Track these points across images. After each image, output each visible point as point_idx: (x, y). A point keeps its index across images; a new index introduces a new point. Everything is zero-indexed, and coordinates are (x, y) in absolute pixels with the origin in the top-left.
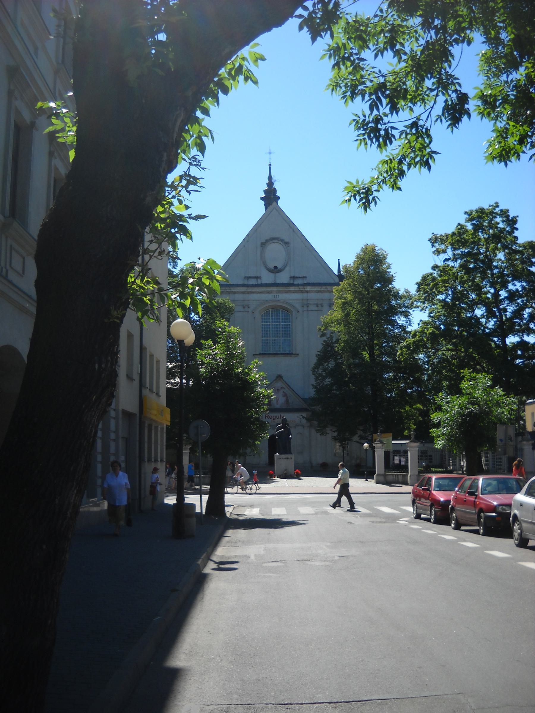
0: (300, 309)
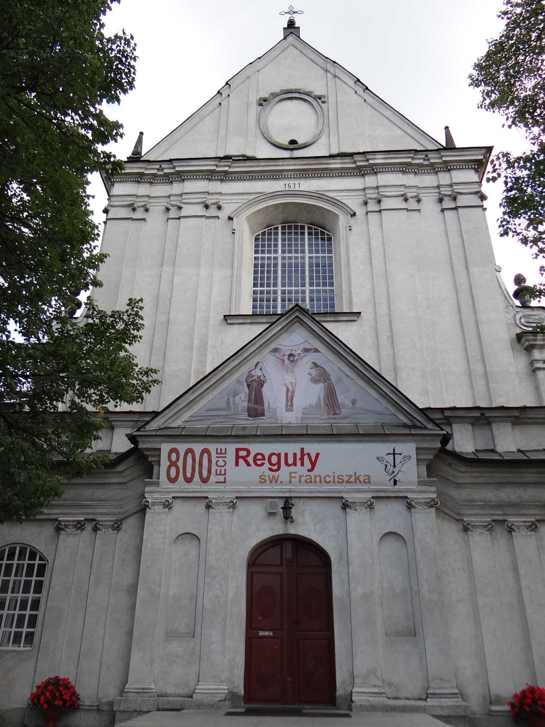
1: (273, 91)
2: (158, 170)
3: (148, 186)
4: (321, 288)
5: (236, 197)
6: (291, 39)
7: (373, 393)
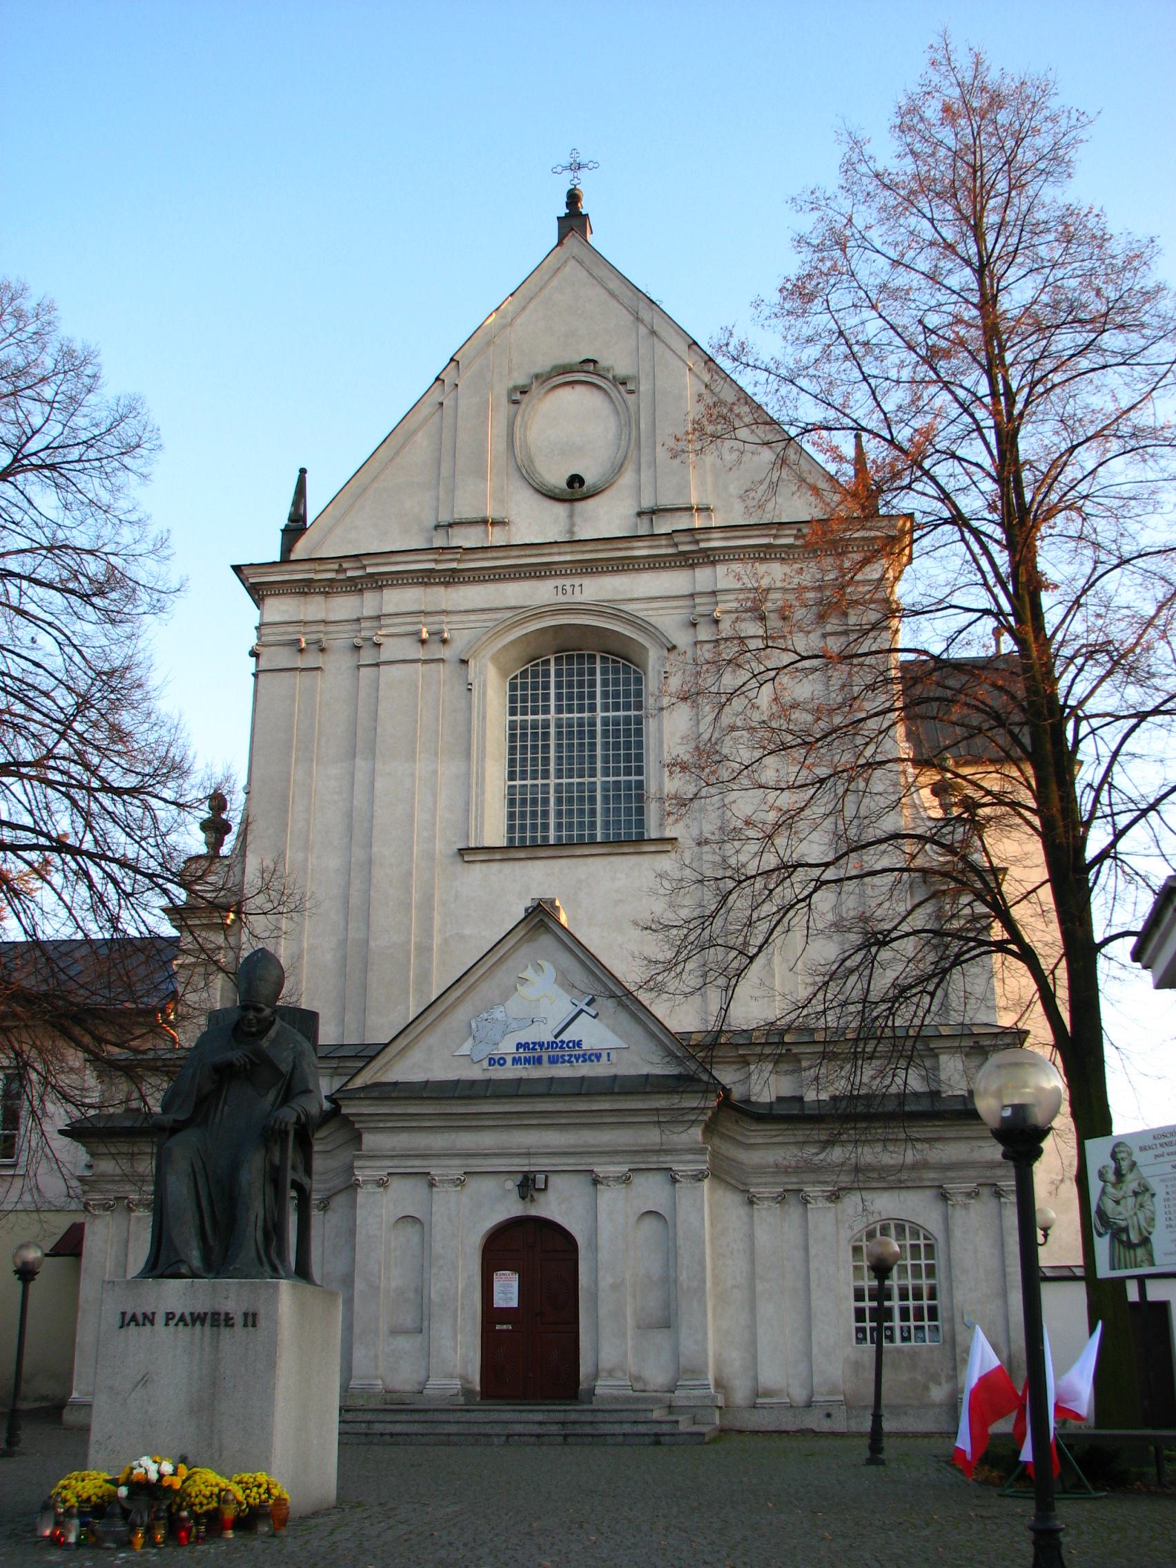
0: (682, 639)
3: (320, 599)
4: (622, 778)
5: (472, 617)
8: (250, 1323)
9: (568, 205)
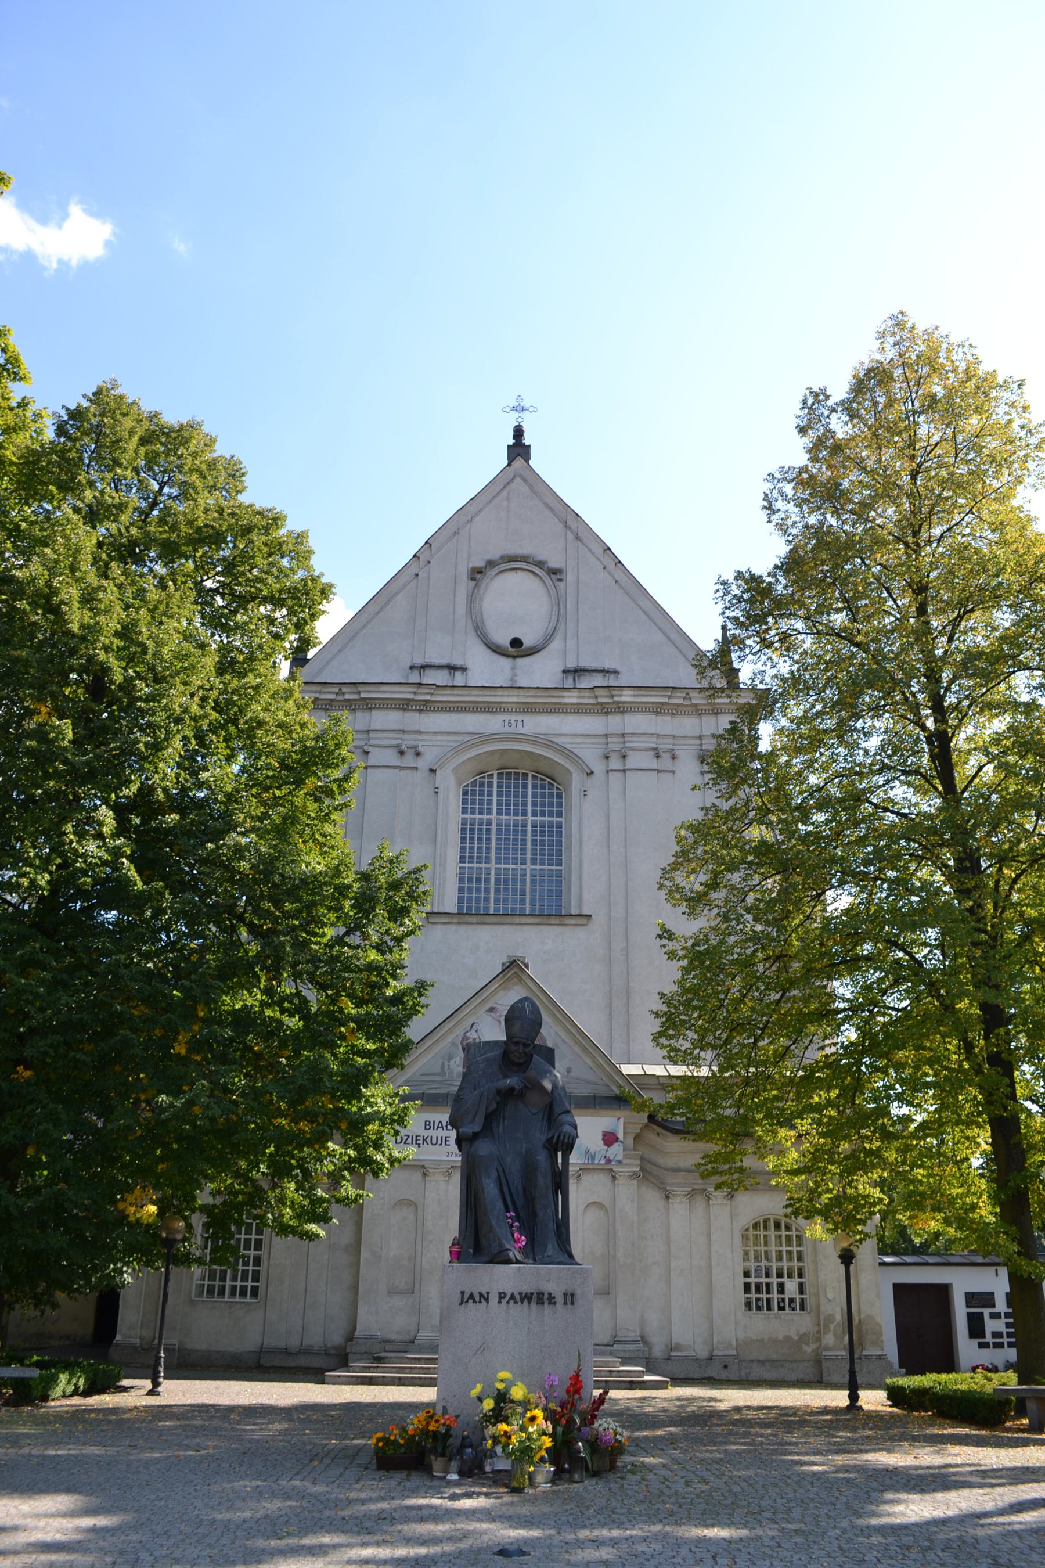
0: (598, 767)
1: (489, 557)
2: (337, 694)
5: (440, 738)
6: (519, 462)
7: (589, 1061)
8: (569, 1302)
9: (514, 437)
